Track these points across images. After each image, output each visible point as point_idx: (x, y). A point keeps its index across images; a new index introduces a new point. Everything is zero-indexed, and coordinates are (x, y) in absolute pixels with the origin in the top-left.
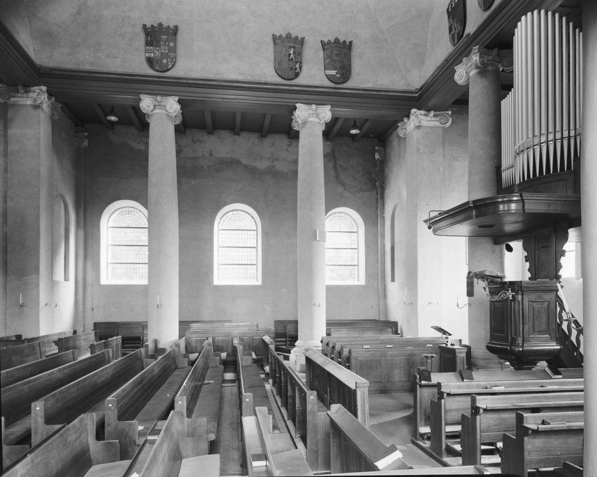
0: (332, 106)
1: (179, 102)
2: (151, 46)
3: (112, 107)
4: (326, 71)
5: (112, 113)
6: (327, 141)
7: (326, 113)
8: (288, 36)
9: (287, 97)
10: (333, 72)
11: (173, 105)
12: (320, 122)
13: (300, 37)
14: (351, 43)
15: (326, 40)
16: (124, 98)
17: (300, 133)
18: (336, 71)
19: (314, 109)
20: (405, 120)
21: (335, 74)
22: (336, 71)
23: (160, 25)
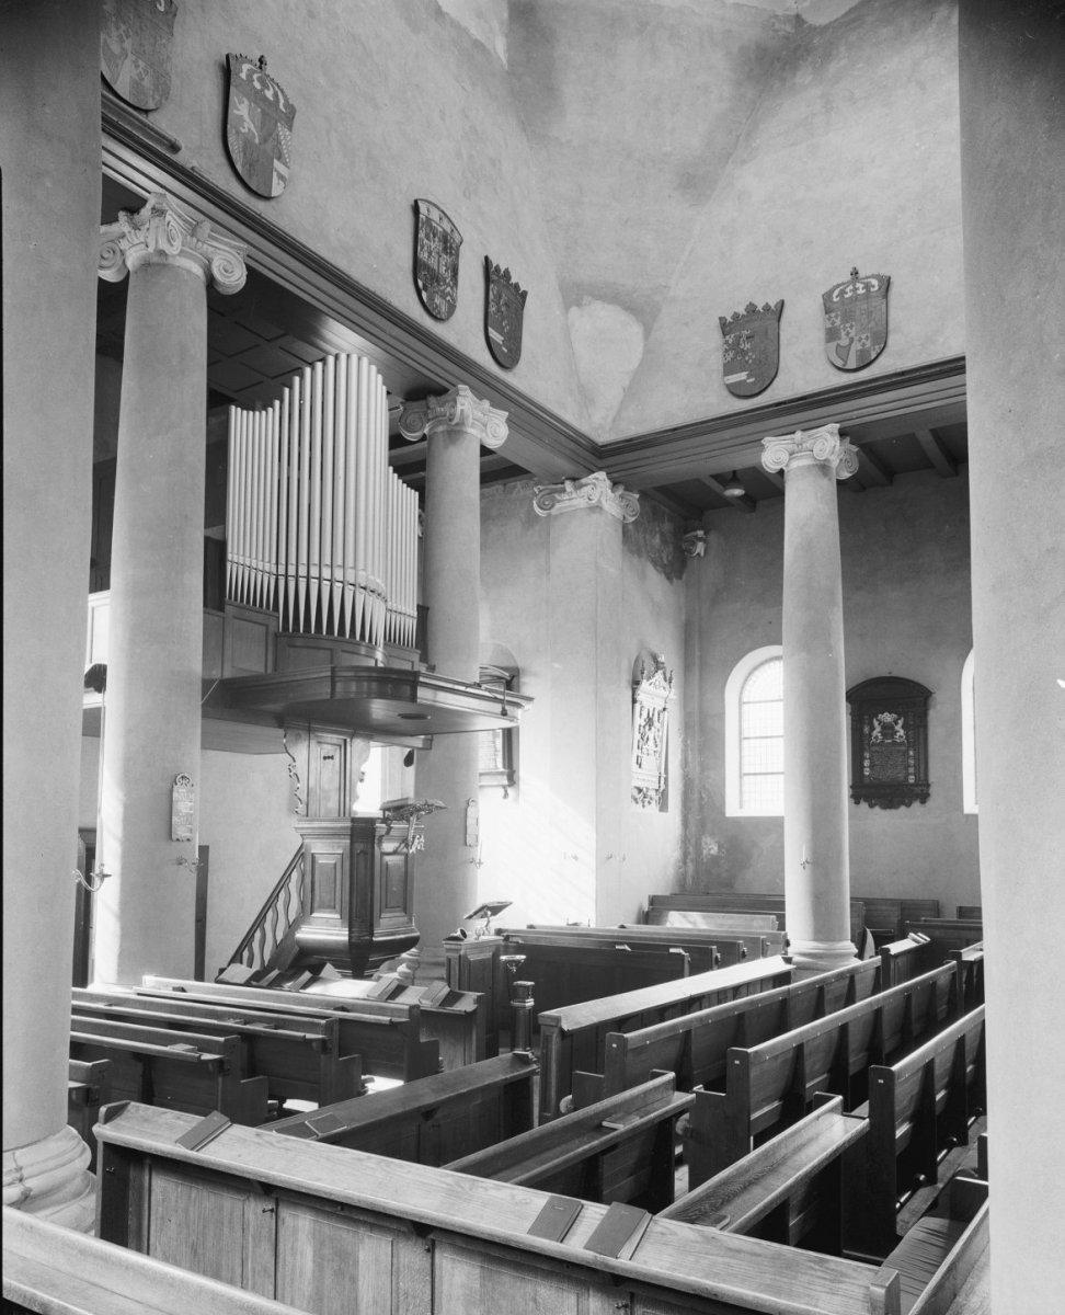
23: (751, 309)
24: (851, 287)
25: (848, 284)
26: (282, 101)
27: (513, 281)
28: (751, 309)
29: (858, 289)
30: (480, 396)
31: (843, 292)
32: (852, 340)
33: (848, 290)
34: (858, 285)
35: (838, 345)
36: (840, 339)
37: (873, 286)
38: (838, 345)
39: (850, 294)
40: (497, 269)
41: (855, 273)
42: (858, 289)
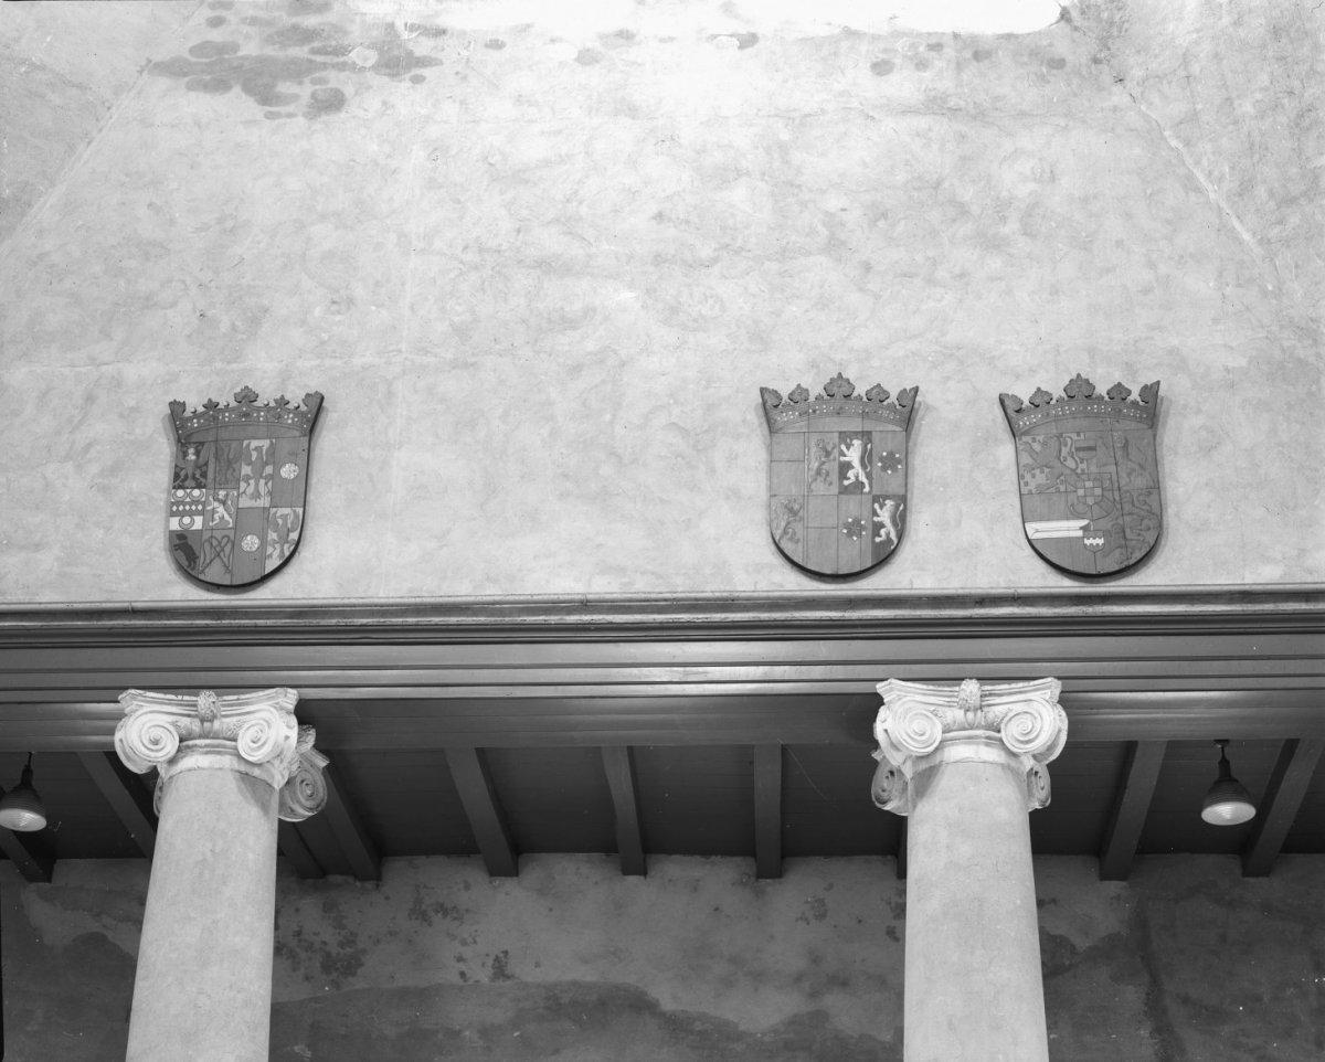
1: (305, 714)
3: (28, 771)
4: (1031, 527)
7: (1037, 718)
10: (1070, 528)
11: (268, 728)
18: (1084, 523)
19: (975, 701)
22: (1084, 523)
30: (943, 676)
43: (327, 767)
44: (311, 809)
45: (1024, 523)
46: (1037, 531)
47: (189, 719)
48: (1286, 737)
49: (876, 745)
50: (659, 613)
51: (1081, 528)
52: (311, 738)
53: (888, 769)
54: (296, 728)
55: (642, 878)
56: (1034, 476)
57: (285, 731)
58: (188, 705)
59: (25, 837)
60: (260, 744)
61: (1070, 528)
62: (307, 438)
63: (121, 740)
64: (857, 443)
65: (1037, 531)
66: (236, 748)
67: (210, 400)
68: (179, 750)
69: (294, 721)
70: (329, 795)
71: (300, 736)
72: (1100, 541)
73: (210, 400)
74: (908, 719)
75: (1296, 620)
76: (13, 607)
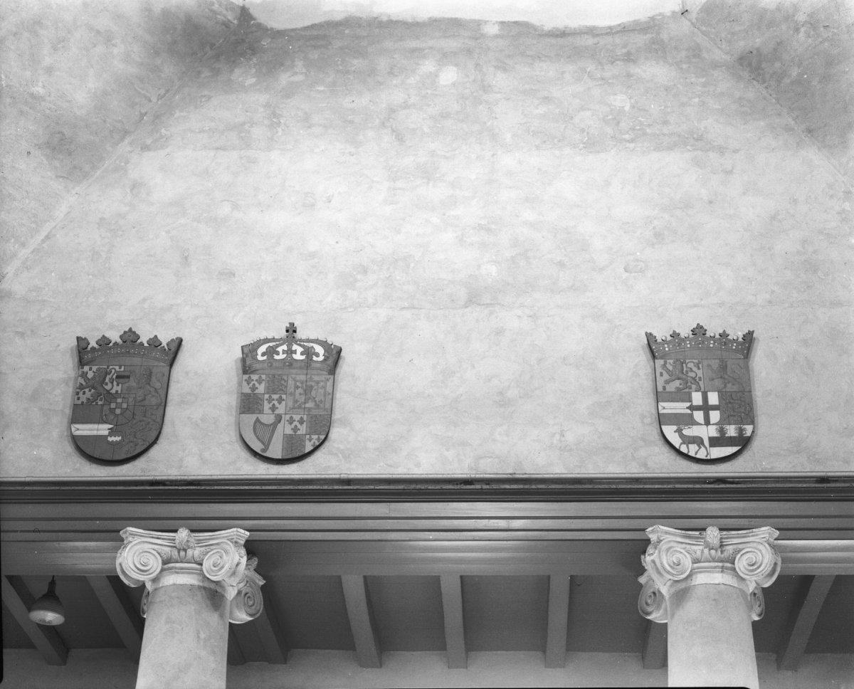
0: (786, 532)
1: (251, 548)
2: (316, 416)
3: (52, 583)
4: (74, 427)
5: (50, 598)
6: (779, 664)
7: (759, 554)
8: (101, 343)
9: (83, 528)
11: (226, 557)
12: (742, 586)
13: (685, 332)
14: (749, 338)
15: (661, 333)
16: (82, 556)
17: (669, 630)
18: (111, 426)
19: (716, 542)
20: (642, 580)
21: (106, 433)
22: (111, 426)
23: (699, 331)
24: (285, 347)
25: (281, 341)
26: (319, 349)
27: (144, 339)
28: (699, 331)
29: (295, 352)
31: (271, 352)
32: (279, 419)
33: (280, 349)
34: (295, 347)
35: (258, 420)
36: (261, 412)
37: (317, 355)
38: (258, 420)
39: (282, 356)
40: (104, 342)
41: (292, 330)
42: (295, 352)
43: (263, 588)
44: (251, 615)
45: (658, 402)
46: (664, 408)
47: (170, 549)
48: (837, 573)
49: (642, 571)
50: (246, 486)
51: (687, 408)
52: (255, 562)
53: (652, 590)
54: (245, 558)
55: (465, 670)
56: (84, 393)
57: (237, 558)
58: (169, 539)
59: (48, 629)
60: (220, 566)
61: (103, 429)
62: (169, 368)
63: (120, 564)
64: (303, 357)
65: (664, 408)
66: (201, 570)
67: (698, 324)
68: (162, 570)
69: (243, 551)
70: (59, 614)
71: (248, 559)
72: (120, 438)
73: (698, 324)
74: (670, 553)
75: (844, 482)
76: (121, 479)
